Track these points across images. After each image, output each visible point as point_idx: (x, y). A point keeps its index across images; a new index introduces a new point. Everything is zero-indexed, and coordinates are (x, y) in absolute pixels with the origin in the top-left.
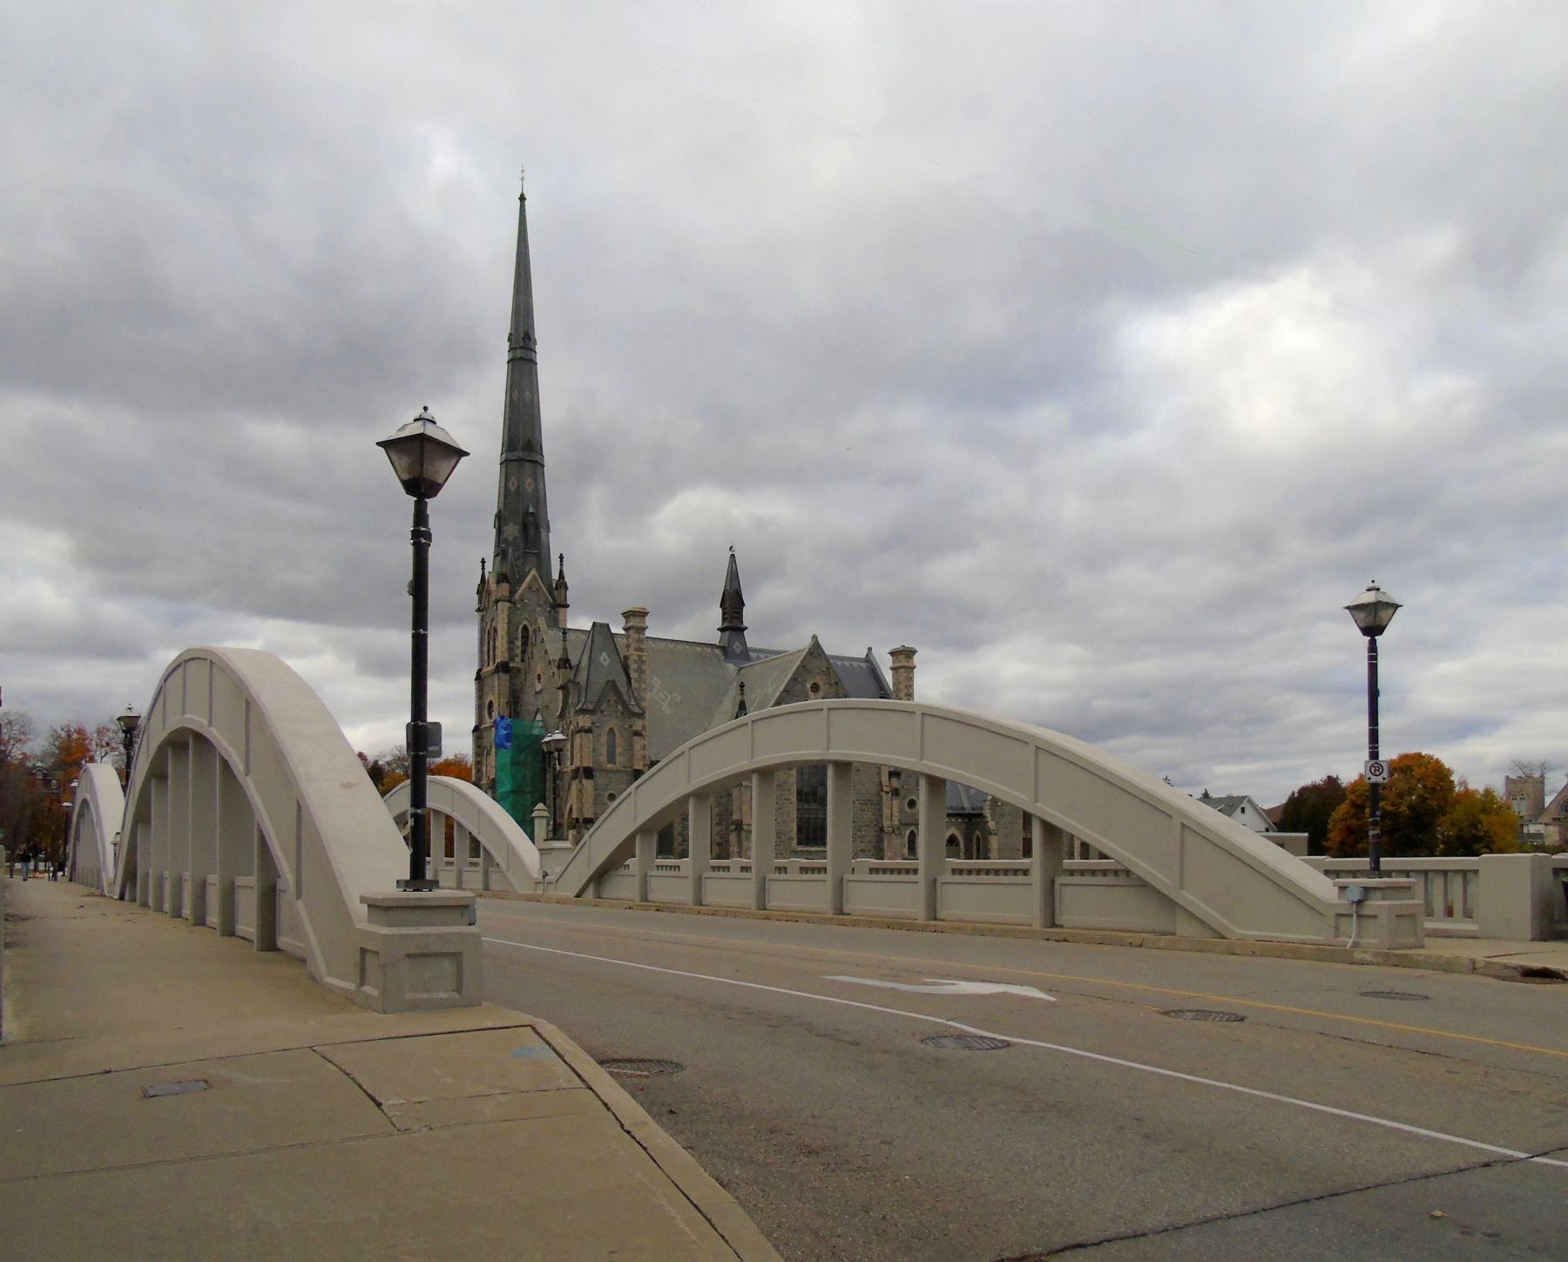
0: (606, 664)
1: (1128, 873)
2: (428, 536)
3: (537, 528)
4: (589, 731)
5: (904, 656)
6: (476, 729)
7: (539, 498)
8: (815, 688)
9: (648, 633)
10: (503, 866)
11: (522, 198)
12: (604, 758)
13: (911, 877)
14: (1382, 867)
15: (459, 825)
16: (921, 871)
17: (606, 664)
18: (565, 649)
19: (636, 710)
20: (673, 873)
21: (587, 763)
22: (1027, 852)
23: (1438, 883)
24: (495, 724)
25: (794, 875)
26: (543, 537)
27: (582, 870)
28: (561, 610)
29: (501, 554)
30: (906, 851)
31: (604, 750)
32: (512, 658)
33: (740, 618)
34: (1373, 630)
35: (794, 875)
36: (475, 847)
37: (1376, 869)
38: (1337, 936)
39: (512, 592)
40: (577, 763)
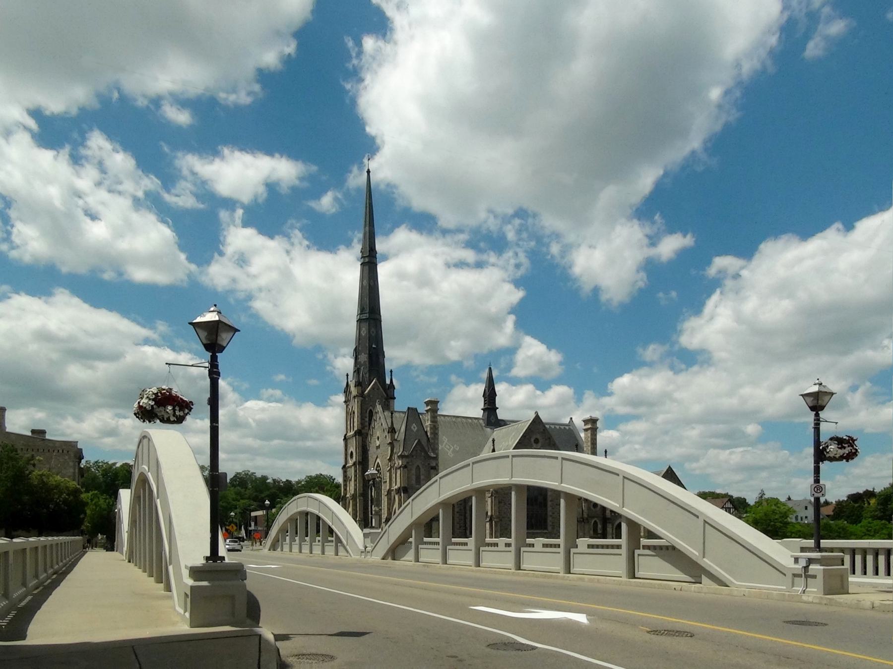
1: (674, 548)
2: (218, 374)
3: (377, 356)
5: (592, 423)
8: (537, 441)
10: (344, 542)
12: (414, 482)
13: (435, 547)
14: (822, 546)
15: (323, 521)
16: (562, 546)
19: (432, 455)
20: (493, 548)
22: (619, 536)
24: (354, 464)
26: (381, 360)
27: (384, 546)
28: (391, 401)
29: (357, 371)
30: (592, 532)
31: (414, 478)
32: (363, 428)
34: (817, 408)
36: (331, 531)
37: (818, 548)
38: (793, 586)
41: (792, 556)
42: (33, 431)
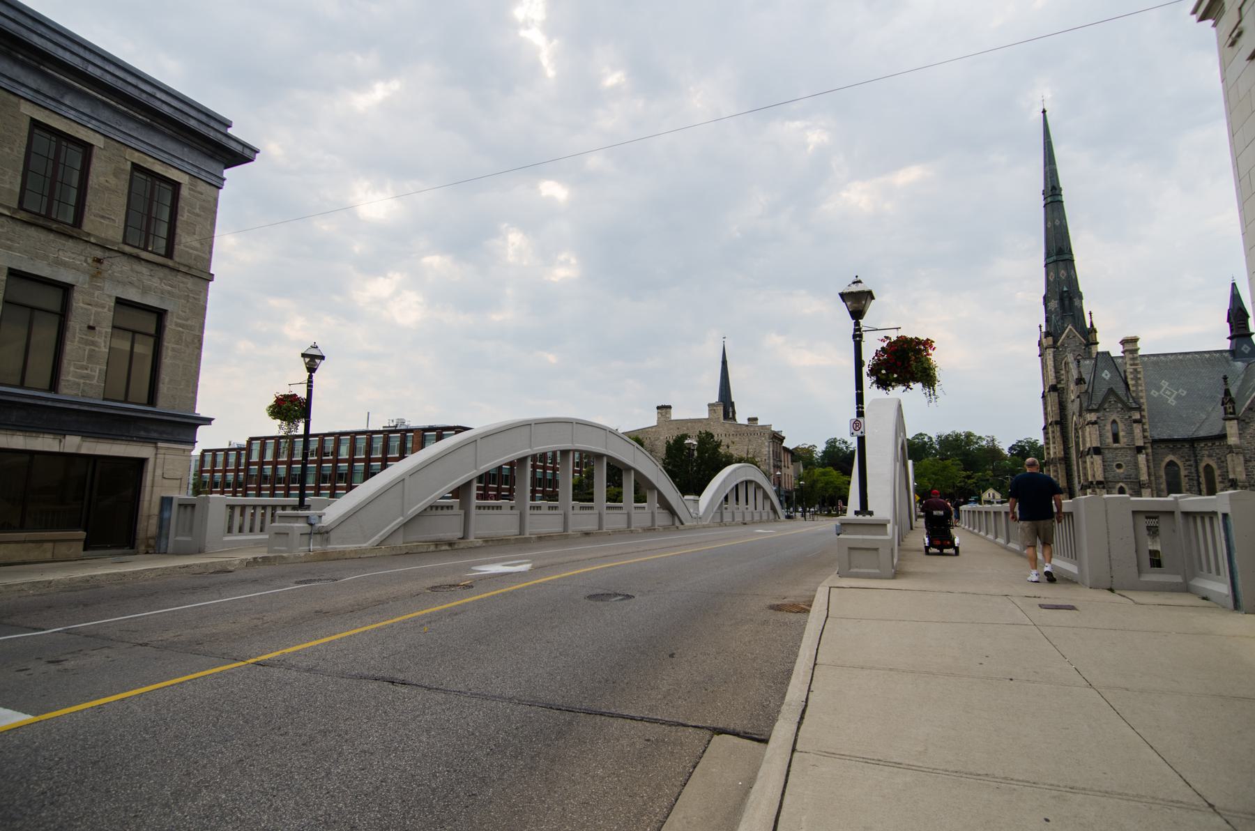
0: (1107, 378)
3: (1071, 299)
4: (1095, 423)
6: (1045, 428)
7: (1073, 282)
9: (1140, 353)
11: (1044, 112)
12: (1110, 440)
17: (1107, 378)
18: (1080, 372)
19: (1134, 405)
21: (1096, 444)
23: (260, 511)
25: (545, 511)
31: (1110, 435)
32: (1059, 382)
33: (1246, 326)
35: (545, 511)
39: (1055, 342)
40: (1088, 445)
41: (871, 513)
42: (749, 419)
